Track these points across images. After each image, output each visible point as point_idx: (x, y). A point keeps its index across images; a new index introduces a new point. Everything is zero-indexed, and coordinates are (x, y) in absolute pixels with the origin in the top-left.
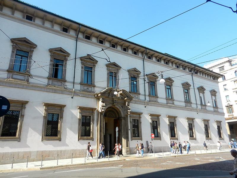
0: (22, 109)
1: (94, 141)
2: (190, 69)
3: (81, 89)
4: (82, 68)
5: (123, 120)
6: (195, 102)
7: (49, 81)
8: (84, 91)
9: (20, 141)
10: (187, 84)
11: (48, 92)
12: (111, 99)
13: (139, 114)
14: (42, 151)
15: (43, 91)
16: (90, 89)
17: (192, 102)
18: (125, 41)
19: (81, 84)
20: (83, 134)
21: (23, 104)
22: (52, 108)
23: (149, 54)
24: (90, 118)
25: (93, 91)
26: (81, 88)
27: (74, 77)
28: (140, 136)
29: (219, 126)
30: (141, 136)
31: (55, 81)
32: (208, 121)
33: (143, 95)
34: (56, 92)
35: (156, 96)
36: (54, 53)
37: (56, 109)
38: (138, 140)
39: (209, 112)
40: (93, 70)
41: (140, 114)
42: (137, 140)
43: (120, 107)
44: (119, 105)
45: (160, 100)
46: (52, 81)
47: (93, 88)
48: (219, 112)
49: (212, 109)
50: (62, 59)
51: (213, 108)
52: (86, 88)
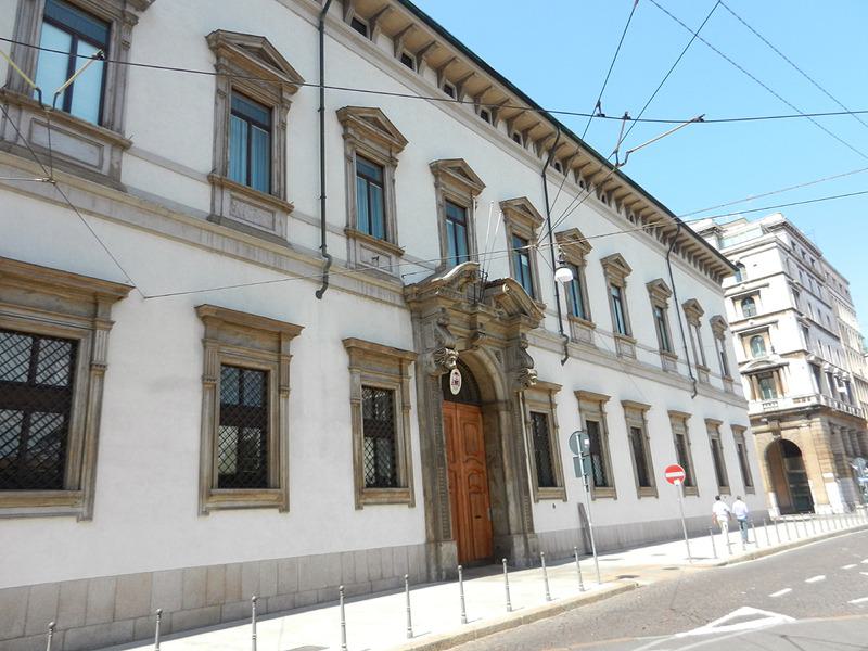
0: (94, 331)
1: (415, 509)
2: (603, 193)
3: (353, 260)
4: (348, 158)
5: (504, 415)
6: (312, 210)
7: (218, 196)
8: (358, 267)
9: (89, 518)
10: (618, 261)
11: (217, 251)
12: (466, 316)
13: (550, 391)
14: (184, 570)
15: (194, 244)
16: (384, 262)
17: (639, 341)
18: (545, 114)
19: (349, 233)
20: (228, 462)
21: (96, 304)
22: (239, 339)
23: (609, 186)
24: (391, 400)
25: (277, 233)
26: (352, 253)
27: (323, 197)
28: (558, 484)
29: (596, 424)
30: (613, 486)
31: (244, 201)
32: (642, 409)
33: (307, 221)
34: (251, 258)
35: (273, 197)
36: (234, 58)
37: (257, 343)
38: (555, 502)
39: (648, 371)
40: (276, 122)
41: (282, 334)
42: (552, 502)
43: (491, 358)
44: (488, 348)
45: (641, 355)
46: (233, 197)
47: (393, 258)
48: (282, 241)
49: (655, 360)
50: (268, 97)
51: (206, 189)
52: (368, 255)
